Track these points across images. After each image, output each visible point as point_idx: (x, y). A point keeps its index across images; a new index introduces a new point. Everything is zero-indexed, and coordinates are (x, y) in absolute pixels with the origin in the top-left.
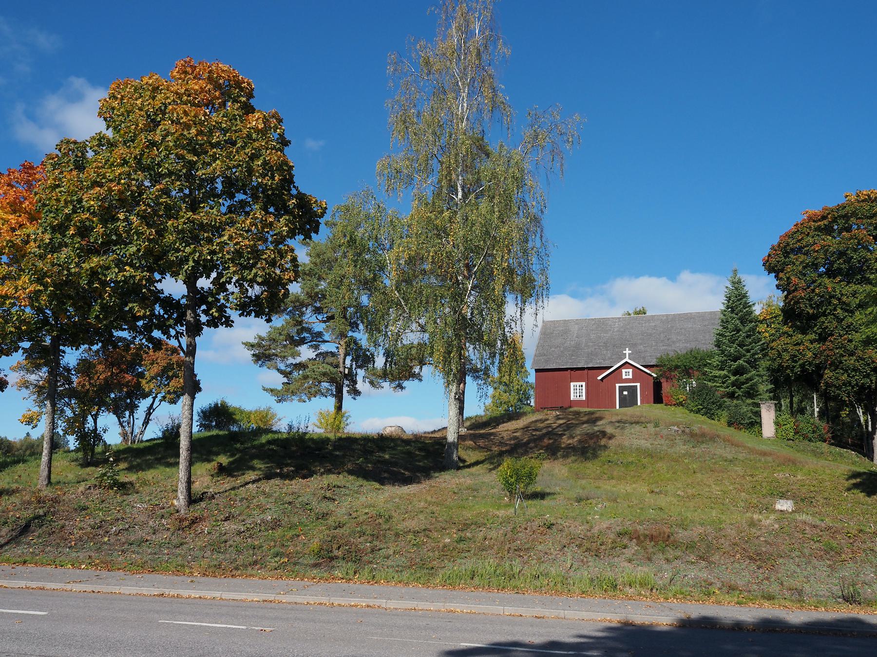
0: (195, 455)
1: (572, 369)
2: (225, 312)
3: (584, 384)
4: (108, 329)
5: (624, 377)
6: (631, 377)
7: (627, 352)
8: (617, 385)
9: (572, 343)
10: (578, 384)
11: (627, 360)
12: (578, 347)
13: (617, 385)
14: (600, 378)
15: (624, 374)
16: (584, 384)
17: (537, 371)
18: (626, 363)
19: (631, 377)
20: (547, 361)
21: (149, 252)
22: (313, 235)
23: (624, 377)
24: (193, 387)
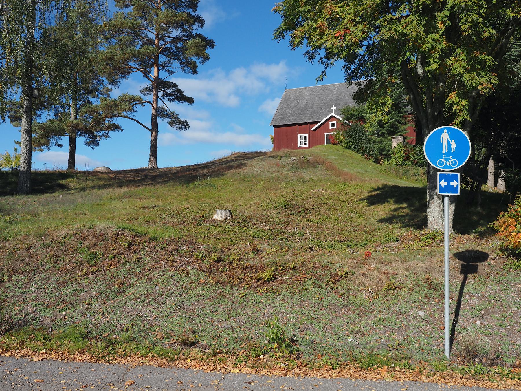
0: (160, 68)
1: (299, 124)
2: (367, 202)
3: (307, 135)
4: (502, 33)
5: (331, 127)
6: (335, 127)
7: (333, 108)
8: (326, 134)
9: (302, 105)
10: (303, 135)
11: (333, 114)
12: (305, 107)
13: (326, 134)
14: (312, 129)
15: (330, 125)
16: (307, 135)
17: (275, 127)
18: (332, 116)
19: (335, 127)
20: (282, 119)
21: (85, 51)
22: (154, 112)
23: (331, 127)
24: (196, 10)
